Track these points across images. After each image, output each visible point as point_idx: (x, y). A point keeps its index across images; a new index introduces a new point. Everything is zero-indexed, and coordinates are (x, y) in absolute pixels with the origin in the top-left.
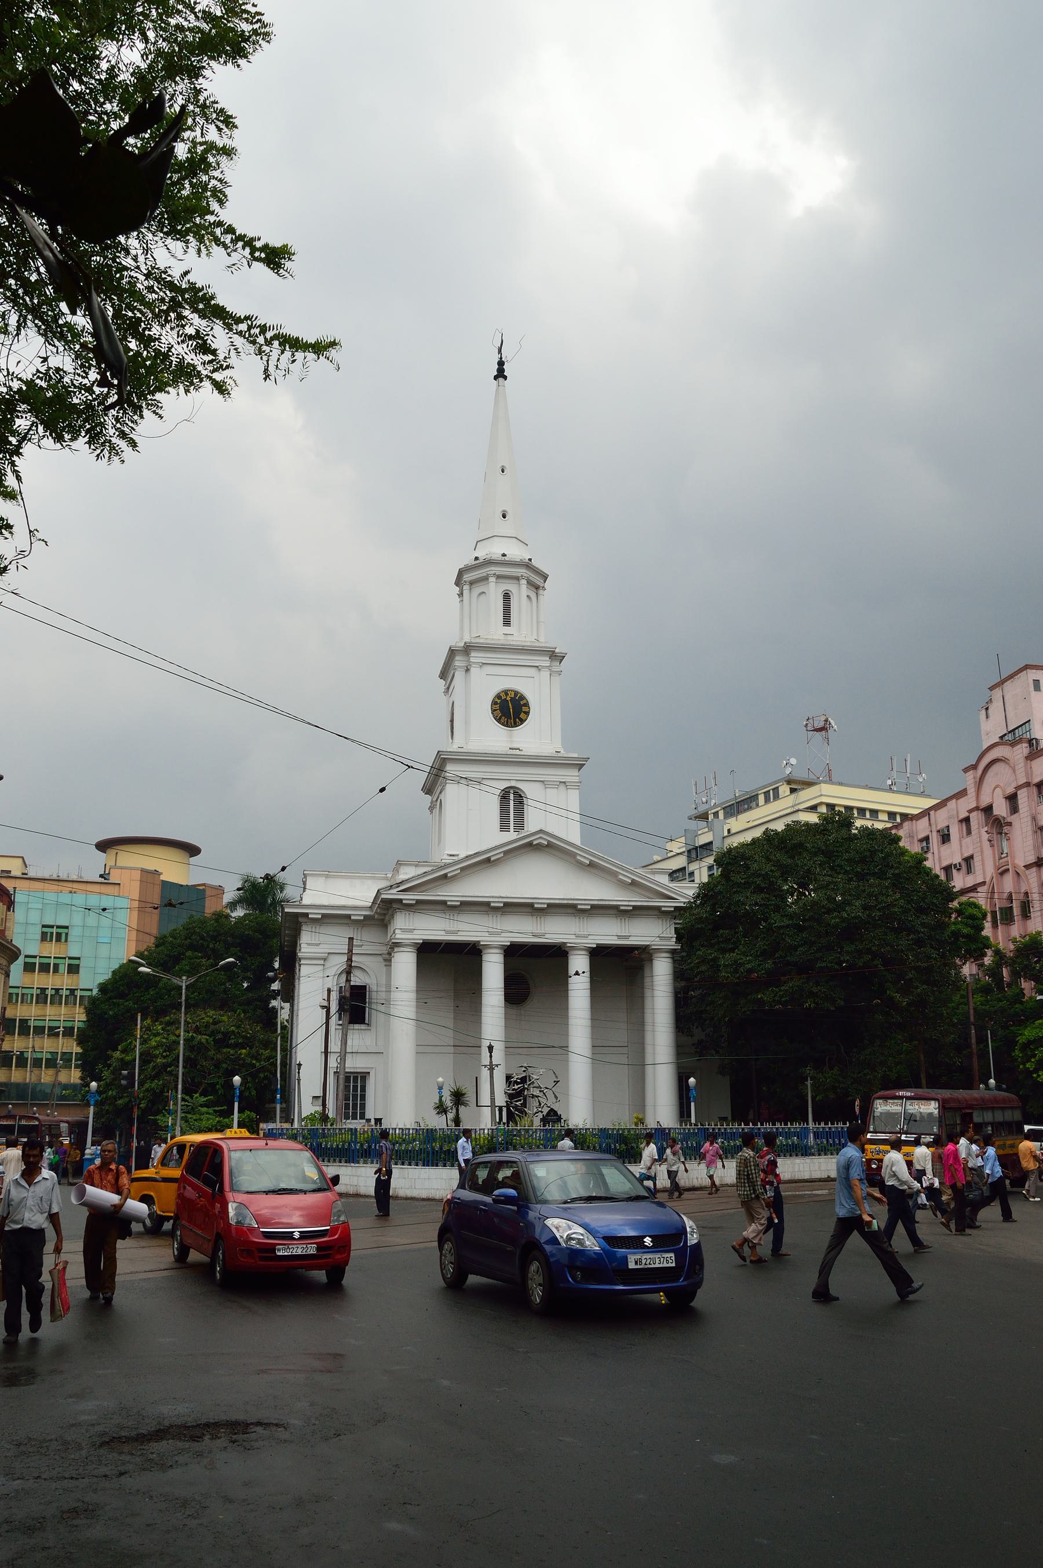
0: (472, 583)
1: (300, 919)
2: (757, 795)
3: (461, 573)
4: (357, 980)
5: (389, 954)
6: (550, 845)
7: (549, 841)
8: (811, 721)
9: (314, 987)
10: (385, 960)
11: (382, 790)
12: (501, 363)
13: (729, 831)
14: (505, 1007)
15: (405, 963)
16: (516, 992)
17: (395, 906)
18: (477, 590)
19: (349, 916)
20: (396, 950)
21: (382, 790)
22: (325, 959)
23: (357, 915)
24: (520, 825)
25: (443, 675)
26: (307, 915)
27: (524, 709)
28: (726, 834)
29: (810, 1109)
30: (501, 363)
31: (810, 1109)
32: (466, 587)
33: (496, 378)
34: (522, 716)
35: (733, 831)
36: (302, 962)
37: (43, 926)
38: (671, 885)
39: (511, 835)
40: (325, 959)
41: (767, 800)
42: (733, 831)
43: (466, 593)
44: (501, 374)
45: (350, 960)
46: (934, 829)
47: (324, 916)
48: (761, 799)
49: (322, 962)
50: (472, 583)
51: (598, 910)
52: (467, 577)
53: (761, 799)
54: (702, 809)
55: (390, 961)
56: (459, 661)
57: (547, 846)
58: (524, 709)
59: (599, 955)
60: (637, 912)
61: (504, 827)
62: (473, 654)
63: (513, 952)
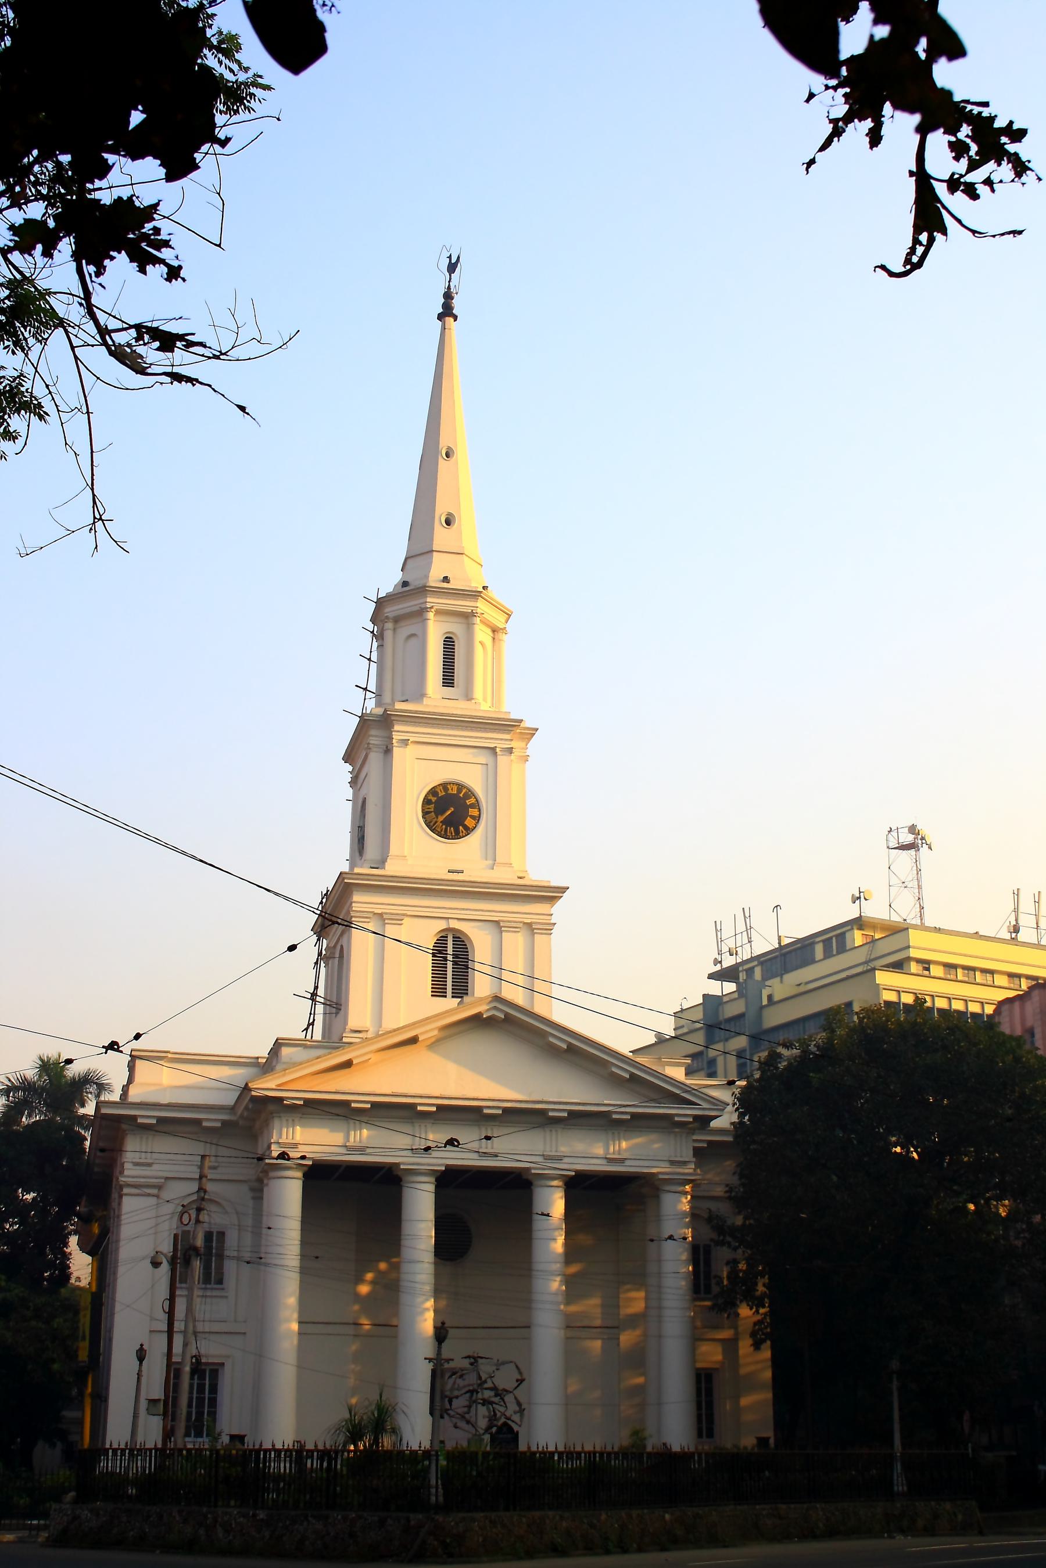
0: (397, 620)
1: (124, 1126)
2: (813, 943)
3: (380, 603)
4: (214, 1218)
5: (260, 1181)
6: (508, 1019)
7: (507, 1014)
8: (894, 834)
9: (143, 1227)
10: (252, 1190)
11: (292, 948)
12: (448, 296)
13: (770, 997)
14: (435, 1263)
15: (289, 1194)
16: (452, 1244)
17: (271, 1107)
18: (405, 630)
19: (197, 1122)
20: (272, 1174)
21: (292, 948)
22: (160, 1187)
23: (211, 1120)
24: (462, 989)
25: (348, 758)
26: (134, 1118)
27: (473, 812)
28: (765, 1002)
29: (897, 1427)
30: (448, 296)
31: (897, 1427)
32: (389, 625)
33: (440, 317)
34: (469, 822)
35: (776, 998)
36: (125, 1190)
37: (226, 1297)
38: (688, 1082)
39: (450, 1002)
40: (160, 1187)
41: (828, 954)
42: (776, 998)
43: (388, 635)
44: (447, 312)
45: (201, 1189)
46: (74, 313)
47: (161, 1120)
48: (819, 950)
49: (155, 1191)
50: (397, 620)
51: (579, 1119)
52: (390, 611)
53: (819, 950)
54: (728, 961)
55: (262, 1191)
56: (375, 738)
57: (628, 1080)
58: (473, 812)
59: (581, 1187)
60: (637, 1123)
61: (438, 991)
62: (397, 728)
63: (449, 1181)
